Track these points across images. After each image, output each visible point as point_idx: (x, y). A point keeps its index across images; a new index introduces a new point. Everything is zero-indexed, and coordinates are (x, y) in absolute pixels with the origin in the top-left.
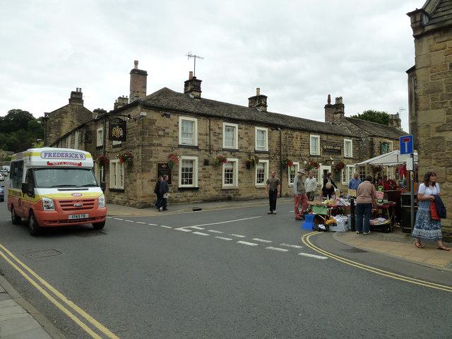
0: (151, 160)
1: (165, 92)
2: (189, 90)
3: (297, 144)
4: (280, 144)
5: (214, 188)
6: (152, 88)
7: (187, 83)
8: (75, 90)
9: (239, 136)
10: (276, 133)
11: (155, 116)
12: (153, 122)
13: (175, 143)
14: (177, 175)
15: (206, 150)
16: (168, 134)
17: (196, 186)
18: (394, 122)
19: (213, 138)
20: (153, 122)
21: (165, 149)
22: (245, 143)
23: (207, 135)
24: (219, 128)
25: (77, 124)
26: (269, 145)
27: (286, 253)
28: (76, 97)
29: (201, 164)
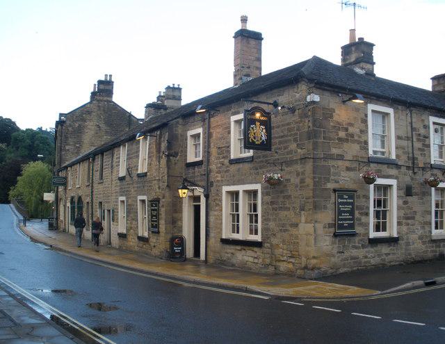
1: (318, 64)
5: (421, 238)
6: (273, 61)
7: (346, 50)
8: (103, 79)
11: (332, 102)
12: (329, 114)
13: (362, 153)
15: (408, 168)
16: (352, 136)
17: (395, 235)
19: (418, 145)
21: (348, 164)
23: (408, 138)
27: (423, 326)
28: (104, 88)
29: (402, 193)
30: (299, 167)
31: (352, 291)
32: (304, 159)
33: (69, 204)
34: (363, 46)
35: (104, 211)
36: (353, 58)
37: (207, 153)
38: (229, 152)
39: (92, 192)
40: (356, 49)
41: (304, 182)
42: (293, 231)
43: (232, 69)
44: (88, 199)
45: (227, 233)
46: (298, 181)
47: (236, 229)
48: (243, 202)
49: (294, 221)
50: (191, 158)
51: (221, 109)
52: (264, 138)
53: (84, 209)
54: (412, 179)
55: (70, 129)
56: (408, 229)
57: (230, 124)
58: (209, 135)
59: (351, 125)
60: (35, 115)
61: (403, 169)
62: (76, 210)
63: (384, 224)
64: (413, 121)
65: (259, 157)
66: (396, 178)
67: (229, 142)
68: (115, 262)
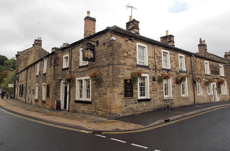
0: (120, 76)
2: (131, 28)
3: (199, 67)
4: (191, 67)
5: (159, 99)
6: (99, 27)
7: (128, 24)
9: (170, 59)
10: (189, 58)
14: (137, 89)
15: (153, 69)
16: (130, 55)
18: (228, 57)
19: (157, 60)
20: (120, 46)
21: (128, 67)
22: (174, 66)
24: (160, 53)
25: (38, 58)
26: (186, 67)
28: (38, 43)
29: (151, 80)
30: (107, 68)
31: (131, 127)
32: (109, 65)
33: (19, 88)
34: (135, 22)
35: (30, 90)
36: (131, 27)
37: (70, 64)
38: (79, 63)
39: (27, 82)
40: (132, 23)
41: (109, 75)
42: (104, 97)
43: (84, 32)
44: (25, 86)
45: (78, 98)
46: (106, 74)
47: (81, 96)
48: (84, 84)
49: (105, 92)
50: (65, 66)
51: (76, 46)
52: (92, 56)
53: (24, 90)
54: (155, 74)
55: (22, 58)
56: (154, 95)
57: (79, 52)
58: (71, 57)
59: (129, 51)
60: (10, 52)
61: (151, 70)
62: (21, 90)
63: (144, 93)
64: (155, 50)
65: (91, 65)
66: (149, 74)
67: (79, 59)
68: (17, 111)
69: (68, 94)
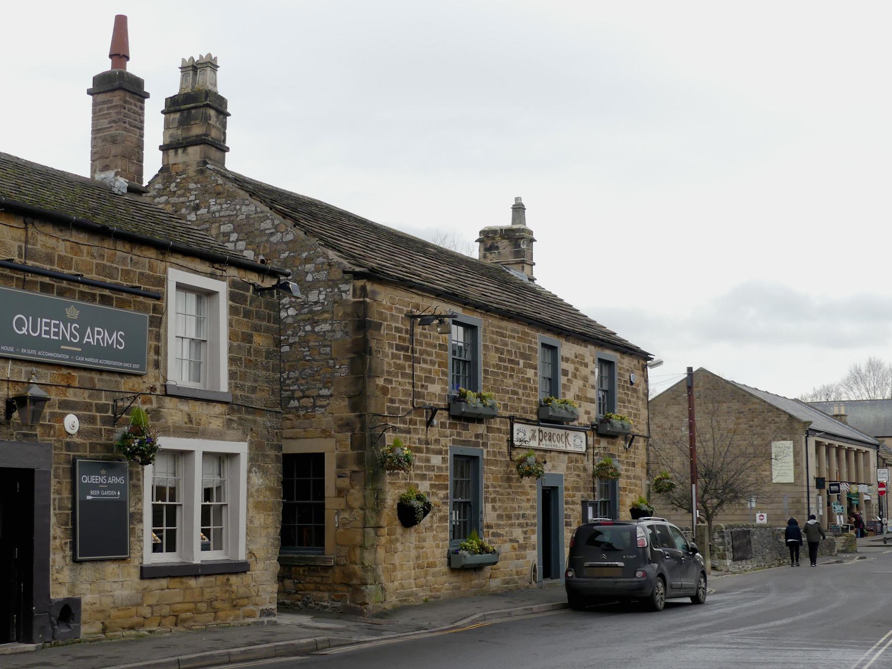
17: (242, 556)
63: (172, 535)
69: (840, 514)
